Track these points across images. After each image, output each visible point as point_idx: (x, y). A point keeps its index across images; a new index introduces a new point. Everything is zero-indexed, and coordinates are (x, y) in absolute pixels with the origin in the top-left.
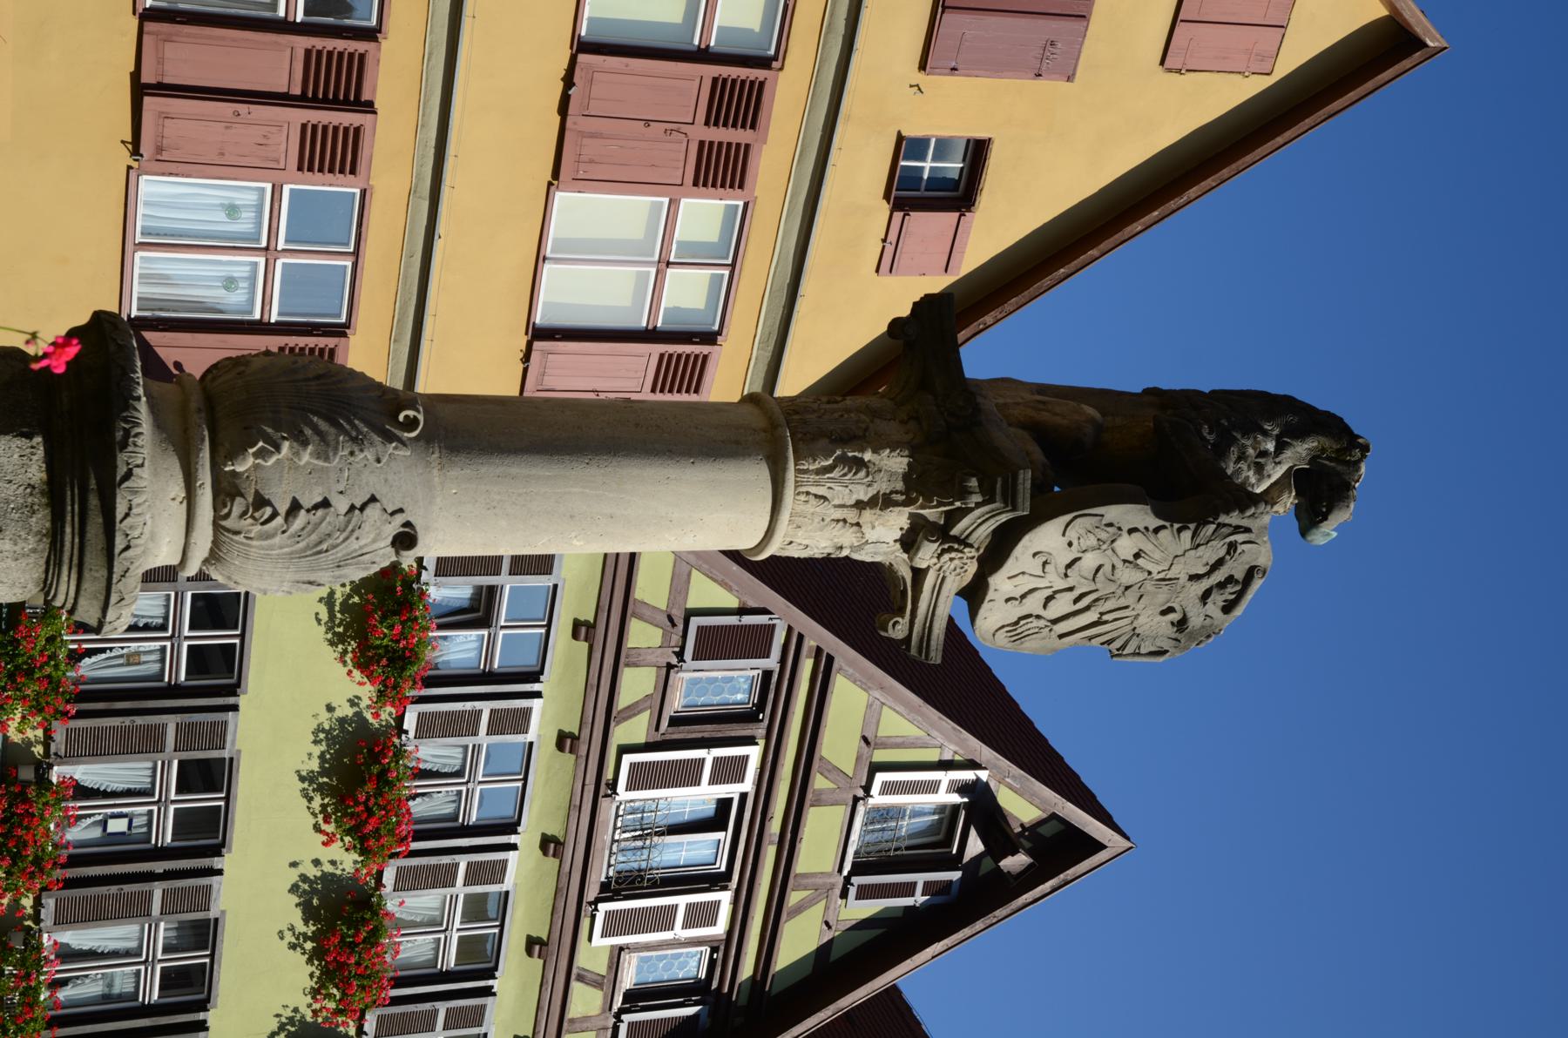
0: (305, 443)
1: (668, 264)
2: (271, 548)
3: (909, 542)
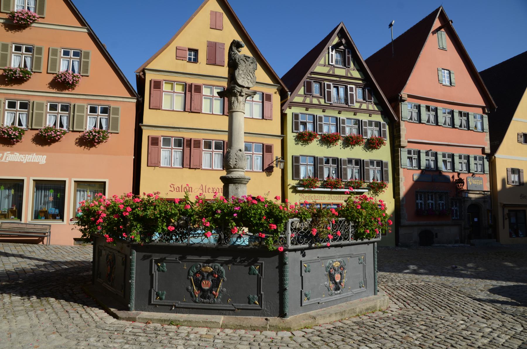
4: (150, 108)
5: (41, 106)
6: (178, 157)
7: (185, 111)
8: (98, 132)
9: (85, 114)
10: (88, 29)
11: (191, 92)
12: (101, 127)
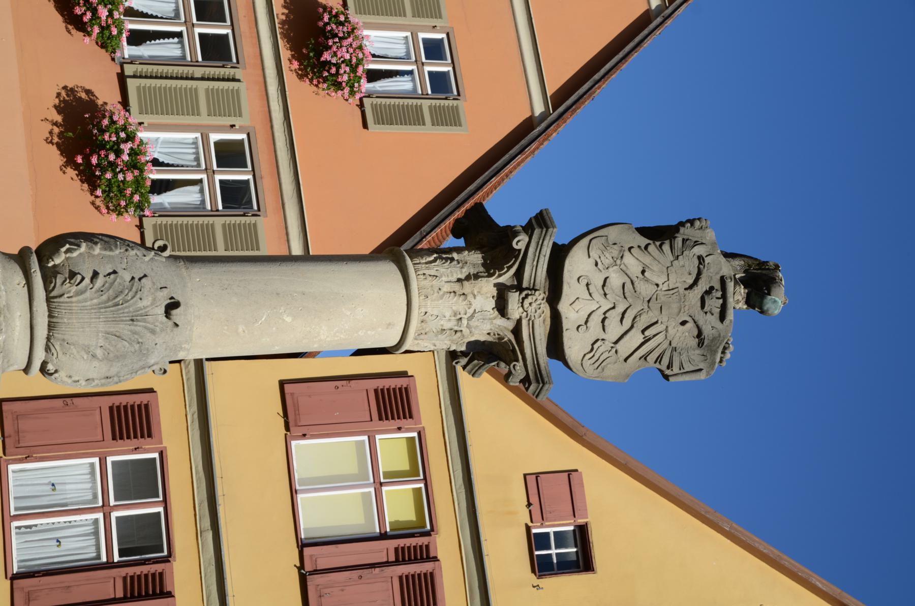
0: (96, 243)
1: (381, 484)
2: (85, 300)
3: (501, 307)
4: (282, 384)
5: (226, 106)
6: (66, 544)
7: (302, 546)
8: (138, 183)
9: (204, 119)
10: (544, 116)
11: (397, 562)
12: (162, 187)
